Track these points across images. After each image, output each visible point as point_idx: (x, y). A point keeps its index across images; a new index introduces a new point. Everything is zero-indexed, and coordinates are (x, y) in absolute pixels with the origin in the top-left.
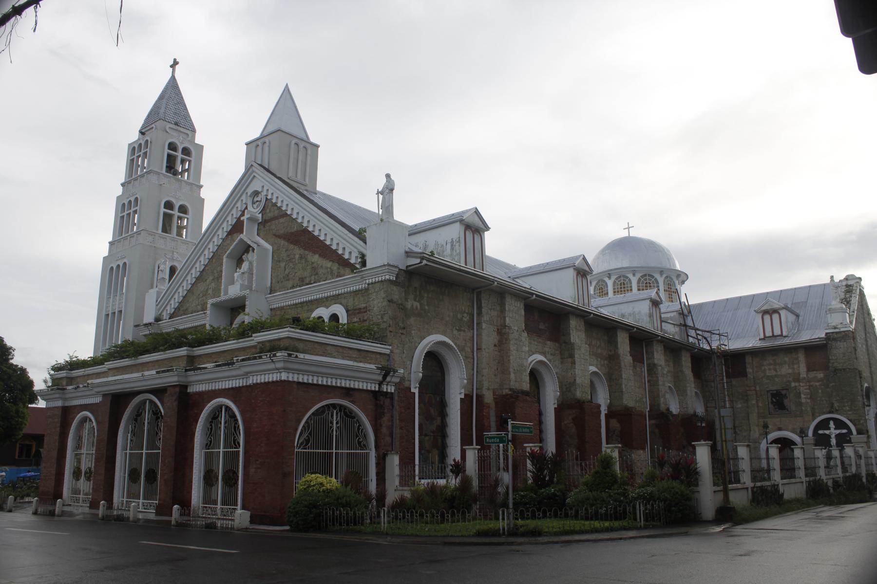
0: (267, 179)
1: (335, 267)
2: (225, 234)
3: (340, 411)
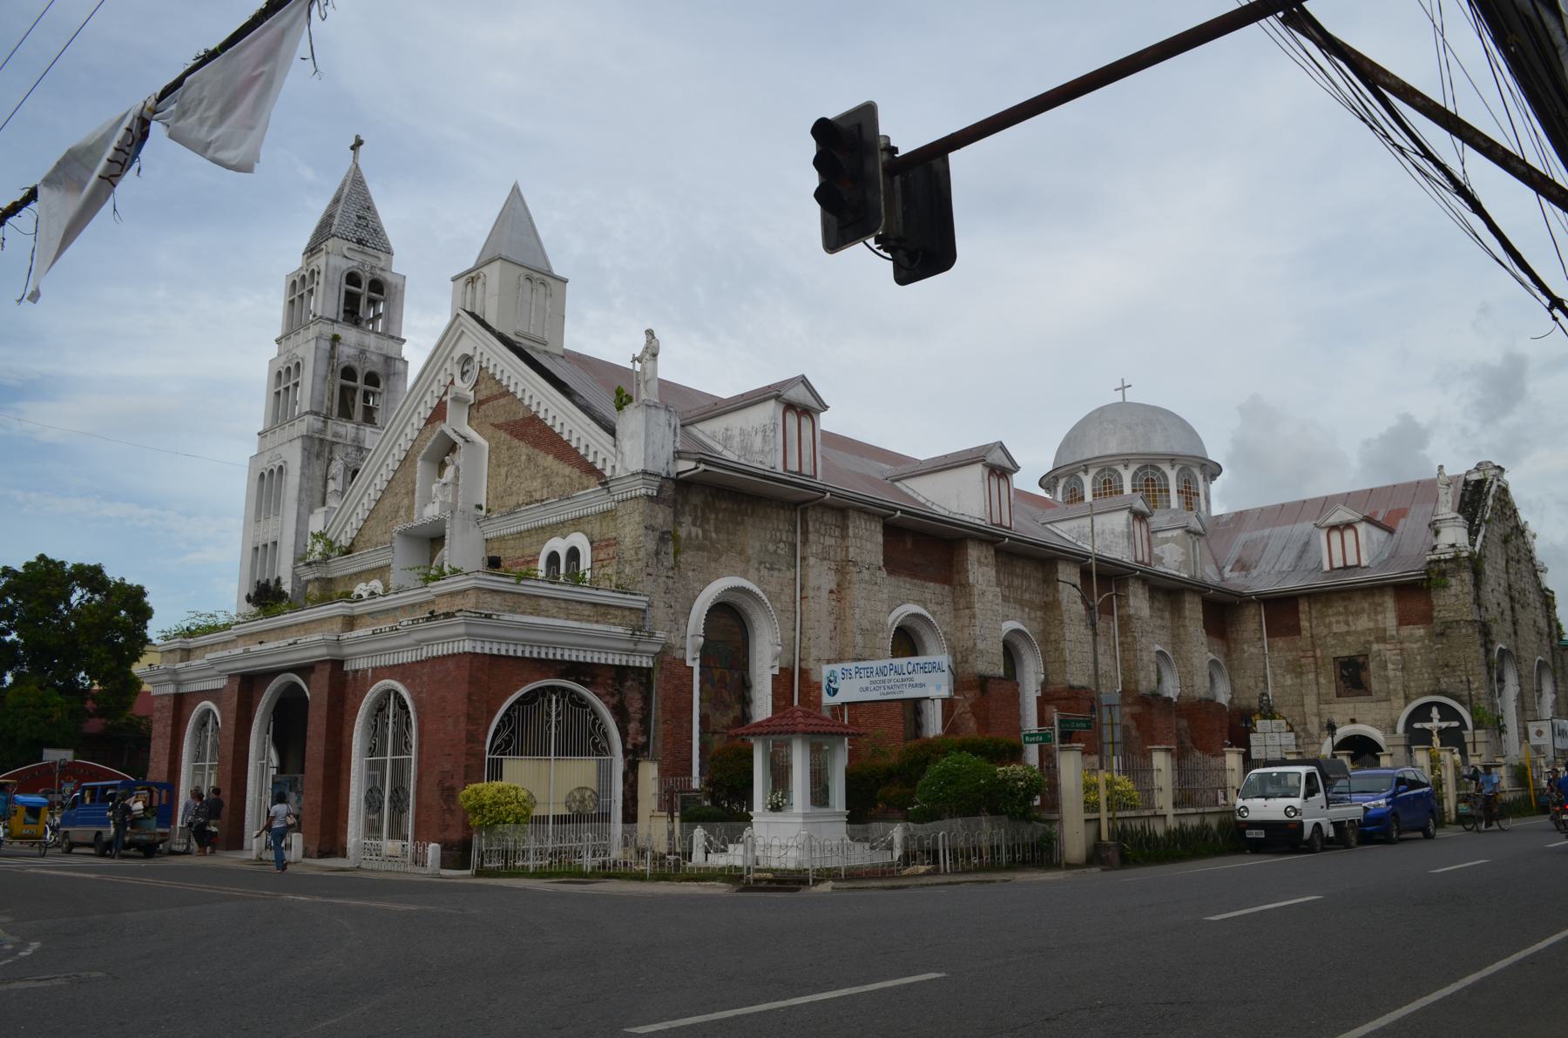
0: (479, 335)
1: (576, 473)
2: (423, 422)
3: (563, 696)
